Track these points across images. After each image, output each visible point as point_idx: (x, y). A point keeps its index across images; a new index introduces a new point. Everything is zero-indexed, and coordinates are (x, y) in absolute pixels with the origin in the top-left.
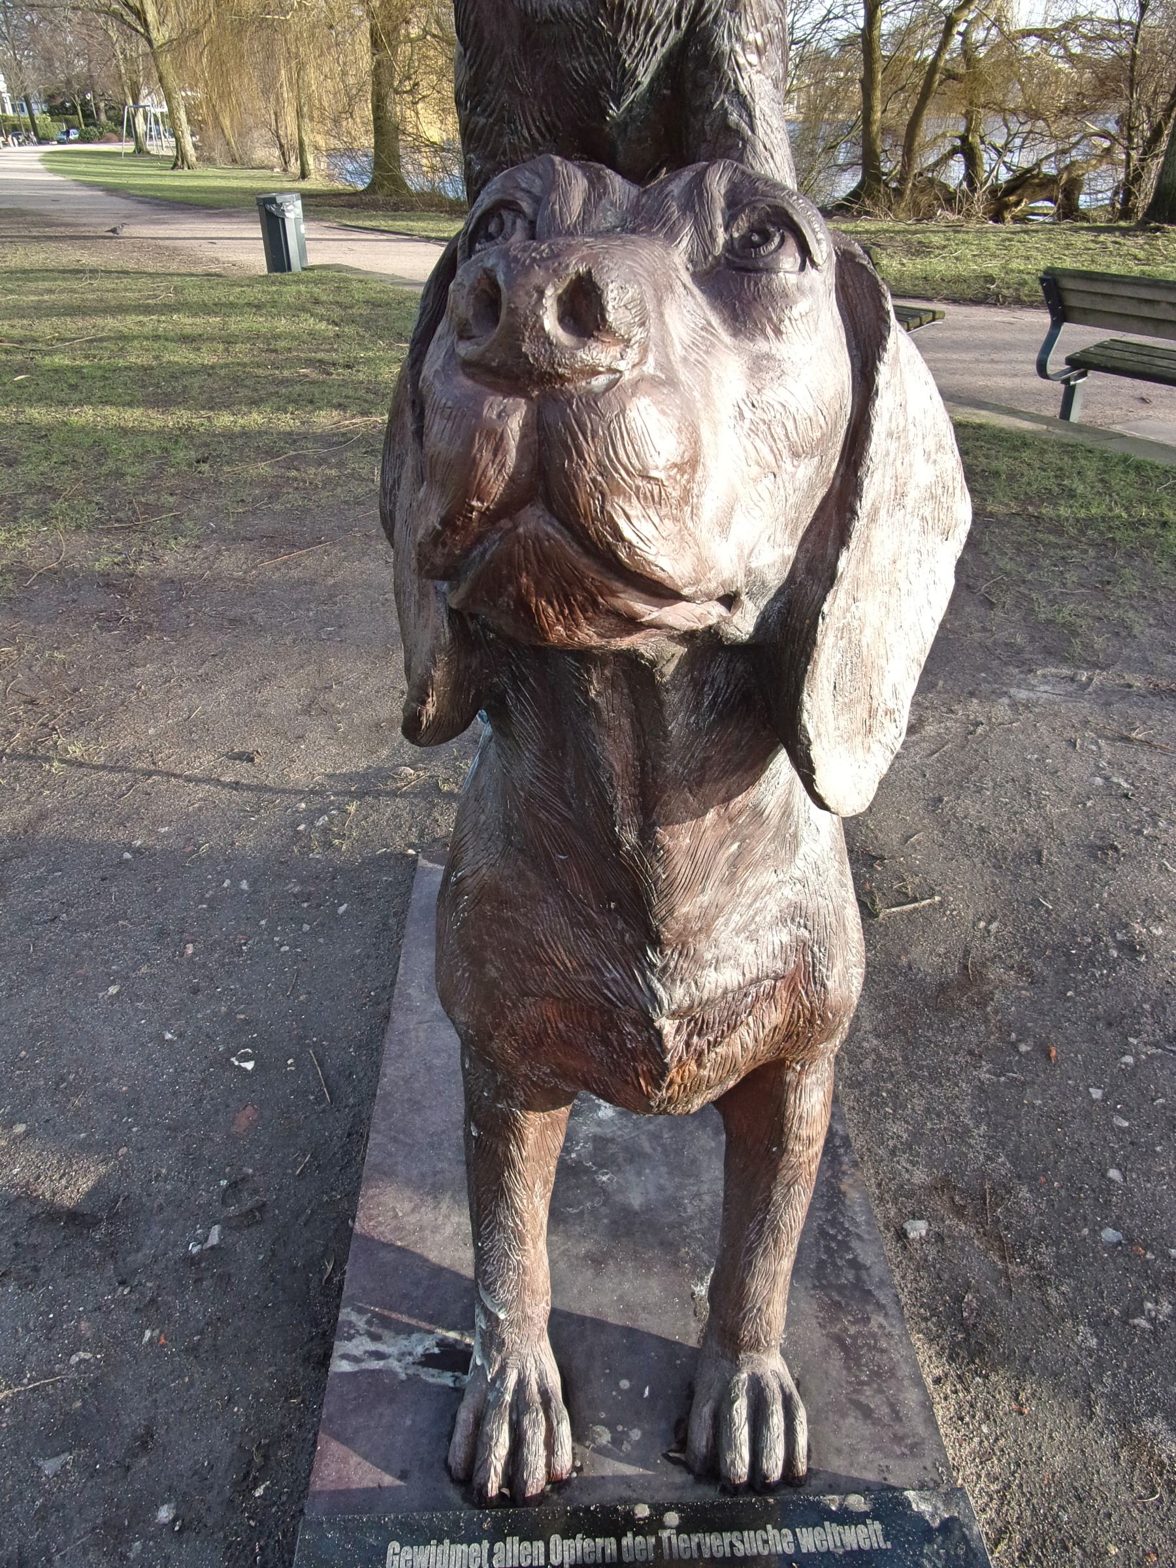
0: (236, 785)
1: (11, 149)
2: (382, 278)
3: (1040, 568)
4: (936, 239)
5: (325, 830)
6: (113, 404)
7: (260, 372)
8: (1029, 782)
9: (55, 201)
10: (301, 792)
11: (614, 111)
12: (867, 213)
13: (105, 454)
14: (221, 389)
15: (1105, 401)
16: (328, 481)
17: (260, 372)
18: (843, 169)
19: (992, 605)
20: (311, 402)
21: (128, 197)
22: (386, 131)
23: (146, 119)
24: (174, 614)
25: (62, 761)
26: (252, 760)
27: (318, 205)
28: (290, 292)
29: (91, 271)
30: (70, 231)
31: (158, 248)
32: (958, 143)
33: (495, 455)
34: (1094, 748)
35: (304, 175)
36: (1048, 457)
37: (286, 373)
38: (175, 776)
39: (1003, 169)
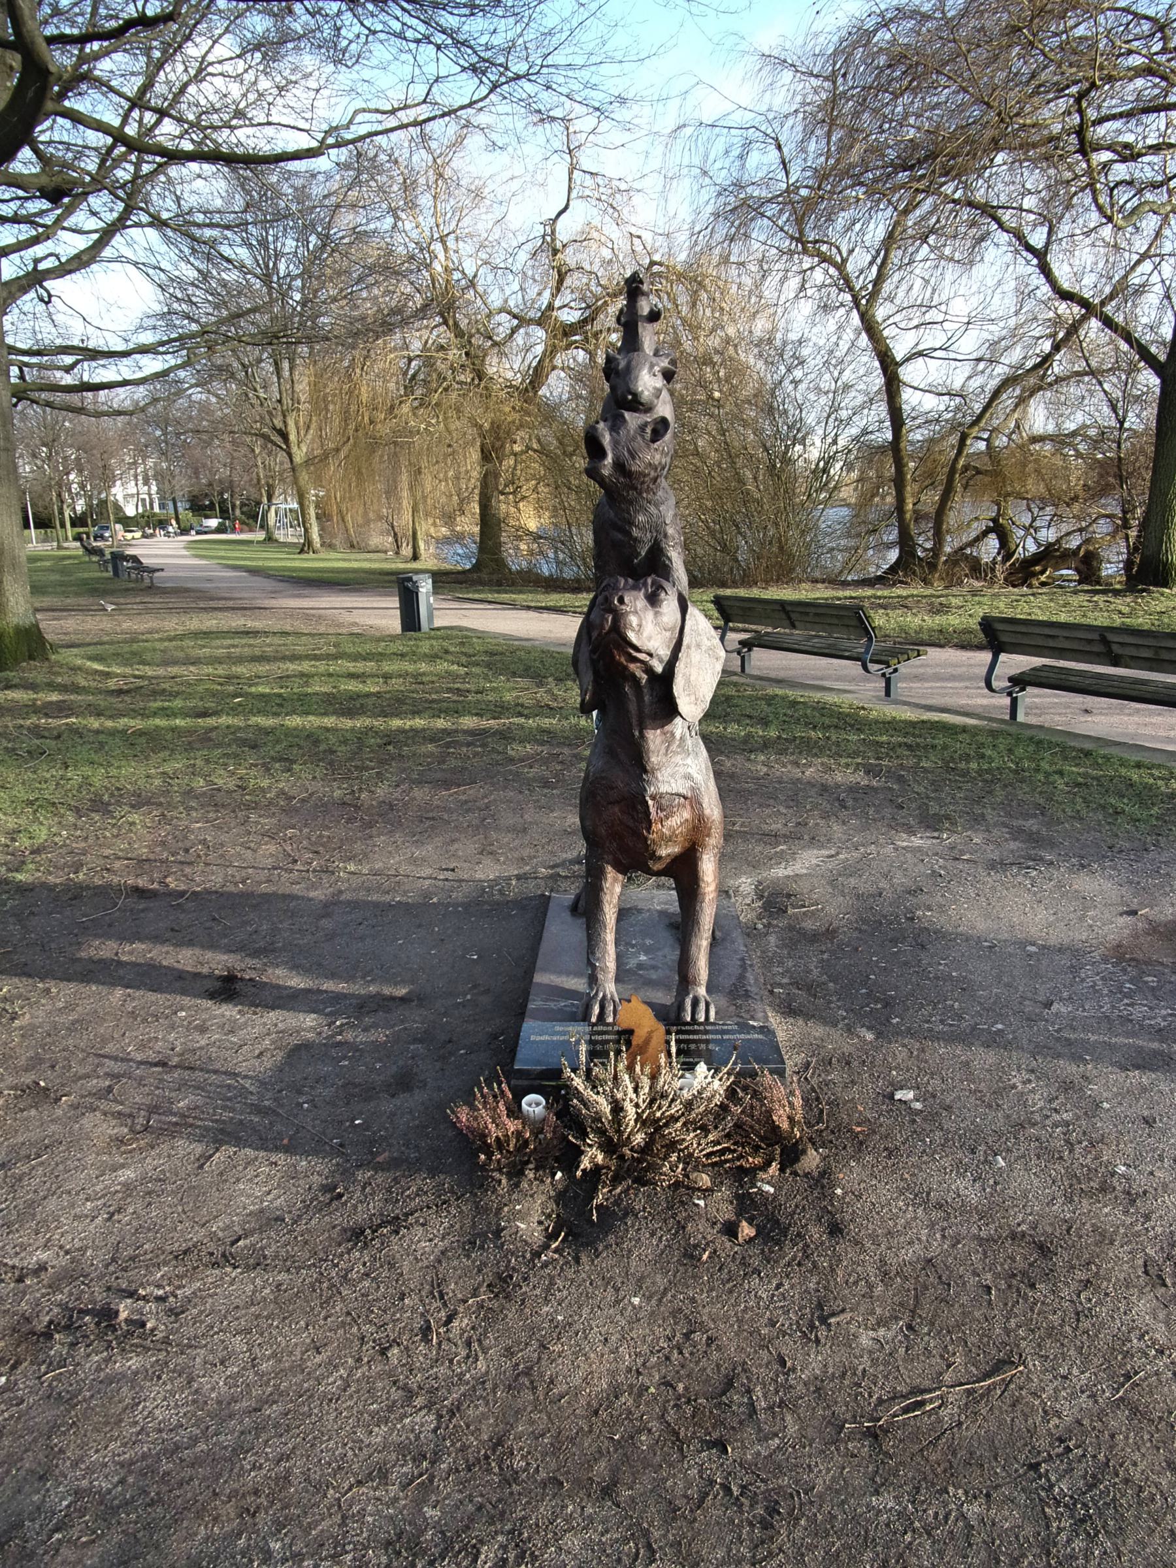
2: (495, 636)
4: (955, 601)
9: (209, 580)
12: (901, 582)
15: (1046, 708)
16: (476, 754)
21: (269, 576)
22: (489, 523)
27: (444, 581)
28: (425, 647)
30: (230, 604)
31: (306, 615)
35: (415, 557)
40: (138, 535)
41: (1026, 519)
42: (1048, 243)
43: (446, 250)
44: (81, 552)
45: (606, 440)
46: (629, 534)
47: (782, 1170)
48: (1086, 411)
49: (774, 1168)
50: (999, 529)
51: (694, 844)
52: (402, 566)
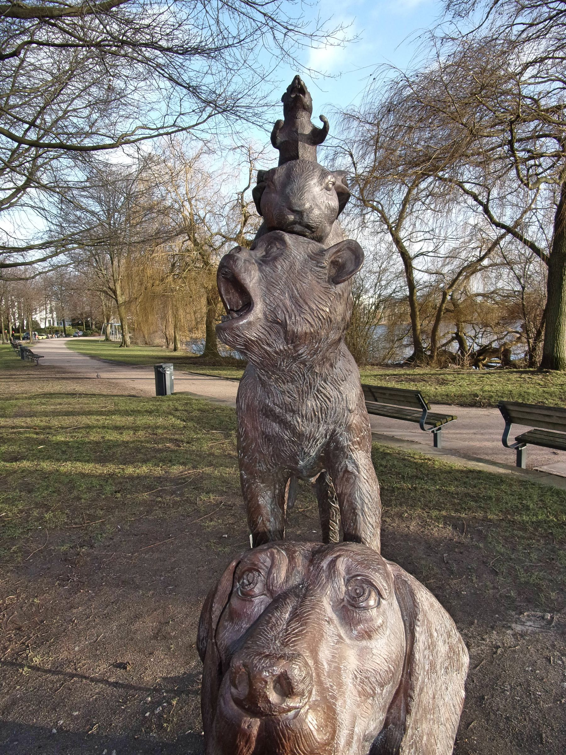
0: (116, 685)
1: (54, 339)
3: (518, 551)
4: (450, 377)
5: (160, 716)
6: (80, 461)
7: (148, 445)
8: (529, 686)
9: (68, 361)
10: (149, 689)
11: (301, 463)
12: (418, 366)
13: (73, 488)
14: (130, 454)
15: (535, 455)
16: (175, 503)
17: (148, 445)
18: (406, 346)
19: (497, 574)
20: (170, 461)
23: (111, 327)
24: (96, 577)
25: (29, 667)
26: (125, 668)
27: (182, 363)
28: (165, 406)
29: (80, 394)
31: (110, 383)
32: (454, 335)
33: (246, 744)
34: (560, 662)
36: (514, 488)
37: (160, 446)
38: (86, 678)
39: (475, 345)
40: (45, 337)
41: (472, 333)
42: (488, 200)
43: (191, 206)
44: (10, 346)
45: (252, 279)
48: (506, 282)
50: (458, 338)
52: (168, 354)
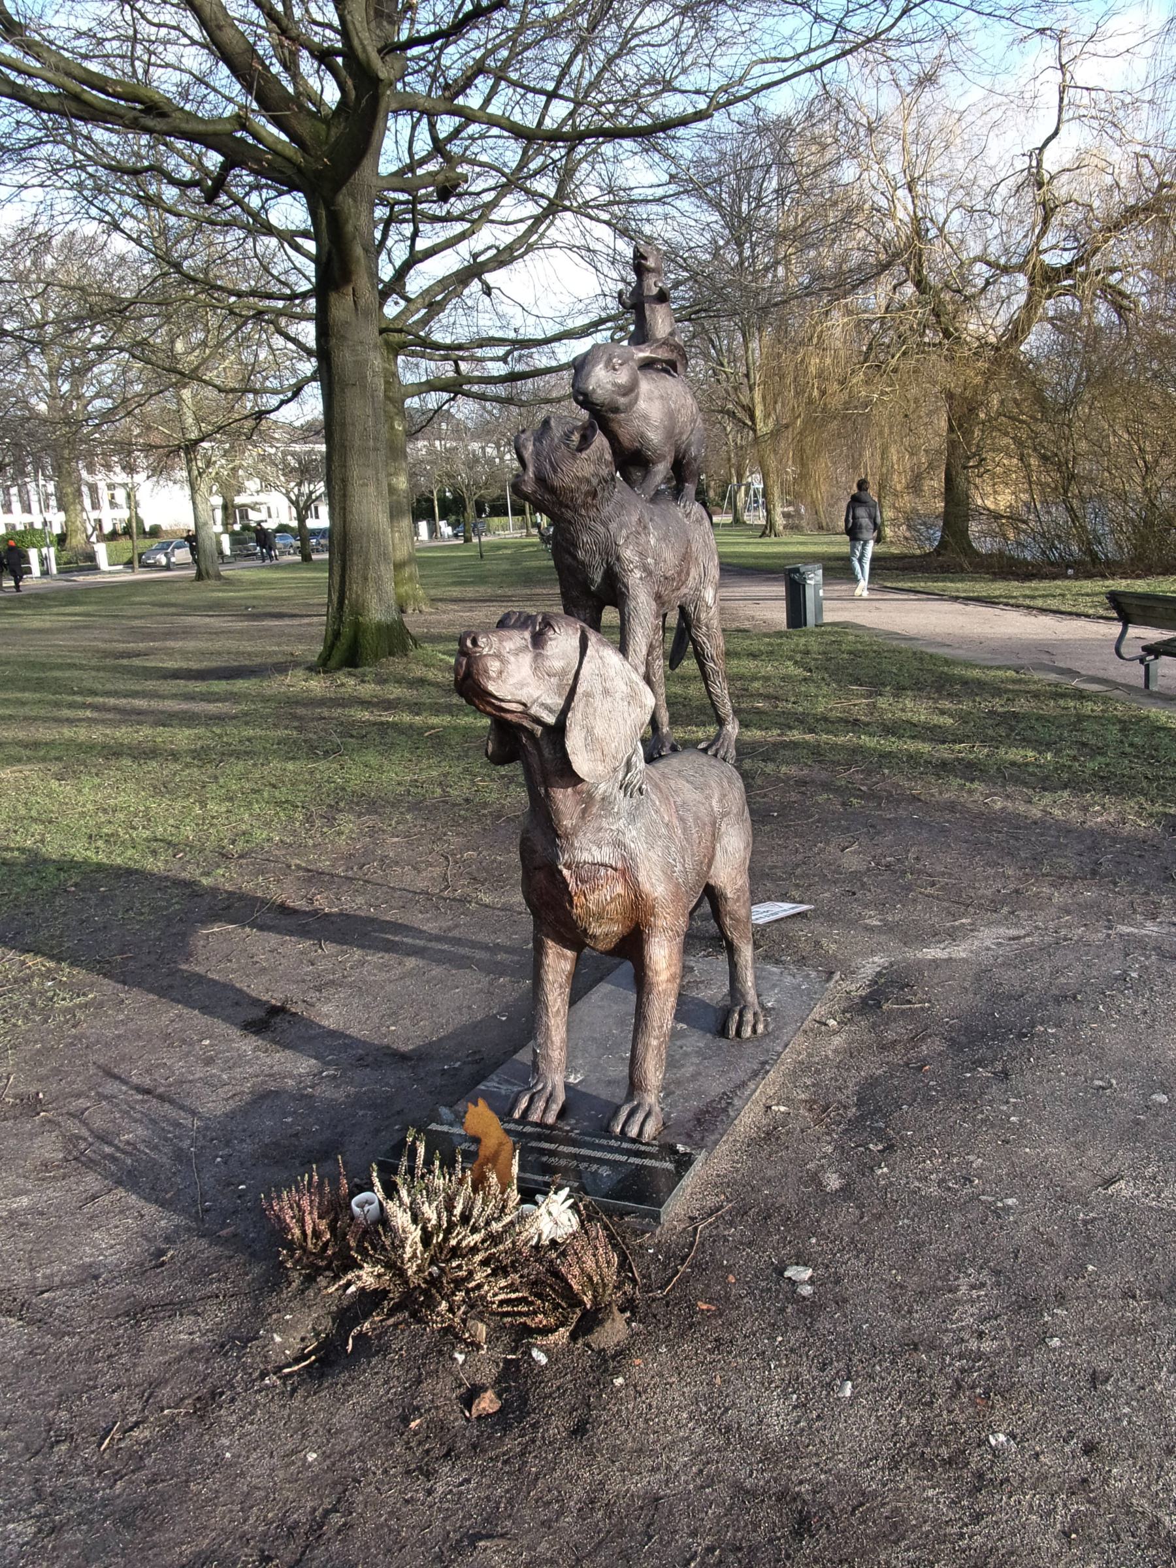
22: (955, 497)
23: (747, 494)
46: (575, 557)
47: (574, 1337)
49: (563, 1333)
51: (638, 924)
